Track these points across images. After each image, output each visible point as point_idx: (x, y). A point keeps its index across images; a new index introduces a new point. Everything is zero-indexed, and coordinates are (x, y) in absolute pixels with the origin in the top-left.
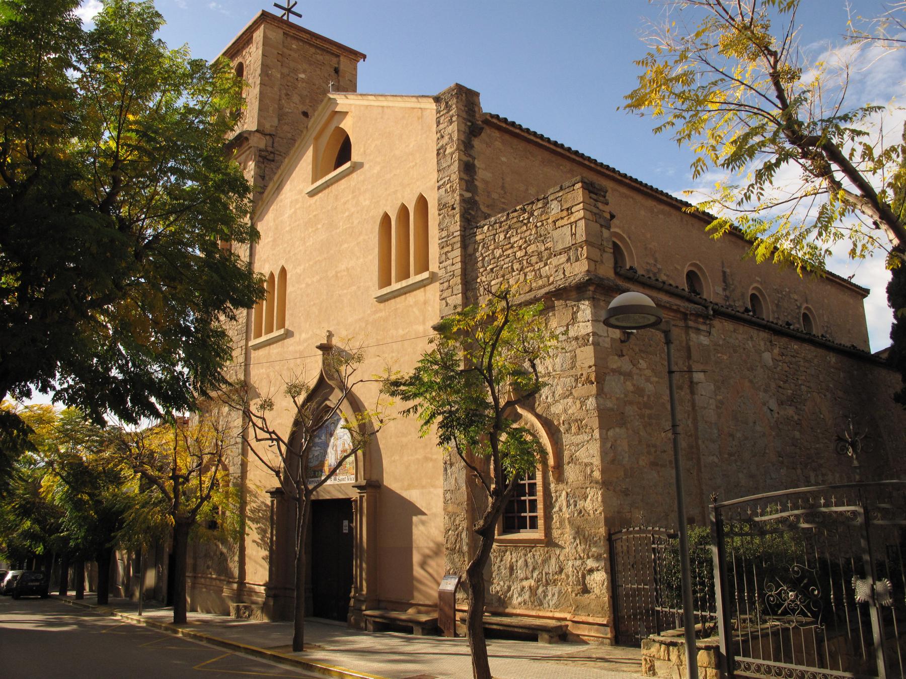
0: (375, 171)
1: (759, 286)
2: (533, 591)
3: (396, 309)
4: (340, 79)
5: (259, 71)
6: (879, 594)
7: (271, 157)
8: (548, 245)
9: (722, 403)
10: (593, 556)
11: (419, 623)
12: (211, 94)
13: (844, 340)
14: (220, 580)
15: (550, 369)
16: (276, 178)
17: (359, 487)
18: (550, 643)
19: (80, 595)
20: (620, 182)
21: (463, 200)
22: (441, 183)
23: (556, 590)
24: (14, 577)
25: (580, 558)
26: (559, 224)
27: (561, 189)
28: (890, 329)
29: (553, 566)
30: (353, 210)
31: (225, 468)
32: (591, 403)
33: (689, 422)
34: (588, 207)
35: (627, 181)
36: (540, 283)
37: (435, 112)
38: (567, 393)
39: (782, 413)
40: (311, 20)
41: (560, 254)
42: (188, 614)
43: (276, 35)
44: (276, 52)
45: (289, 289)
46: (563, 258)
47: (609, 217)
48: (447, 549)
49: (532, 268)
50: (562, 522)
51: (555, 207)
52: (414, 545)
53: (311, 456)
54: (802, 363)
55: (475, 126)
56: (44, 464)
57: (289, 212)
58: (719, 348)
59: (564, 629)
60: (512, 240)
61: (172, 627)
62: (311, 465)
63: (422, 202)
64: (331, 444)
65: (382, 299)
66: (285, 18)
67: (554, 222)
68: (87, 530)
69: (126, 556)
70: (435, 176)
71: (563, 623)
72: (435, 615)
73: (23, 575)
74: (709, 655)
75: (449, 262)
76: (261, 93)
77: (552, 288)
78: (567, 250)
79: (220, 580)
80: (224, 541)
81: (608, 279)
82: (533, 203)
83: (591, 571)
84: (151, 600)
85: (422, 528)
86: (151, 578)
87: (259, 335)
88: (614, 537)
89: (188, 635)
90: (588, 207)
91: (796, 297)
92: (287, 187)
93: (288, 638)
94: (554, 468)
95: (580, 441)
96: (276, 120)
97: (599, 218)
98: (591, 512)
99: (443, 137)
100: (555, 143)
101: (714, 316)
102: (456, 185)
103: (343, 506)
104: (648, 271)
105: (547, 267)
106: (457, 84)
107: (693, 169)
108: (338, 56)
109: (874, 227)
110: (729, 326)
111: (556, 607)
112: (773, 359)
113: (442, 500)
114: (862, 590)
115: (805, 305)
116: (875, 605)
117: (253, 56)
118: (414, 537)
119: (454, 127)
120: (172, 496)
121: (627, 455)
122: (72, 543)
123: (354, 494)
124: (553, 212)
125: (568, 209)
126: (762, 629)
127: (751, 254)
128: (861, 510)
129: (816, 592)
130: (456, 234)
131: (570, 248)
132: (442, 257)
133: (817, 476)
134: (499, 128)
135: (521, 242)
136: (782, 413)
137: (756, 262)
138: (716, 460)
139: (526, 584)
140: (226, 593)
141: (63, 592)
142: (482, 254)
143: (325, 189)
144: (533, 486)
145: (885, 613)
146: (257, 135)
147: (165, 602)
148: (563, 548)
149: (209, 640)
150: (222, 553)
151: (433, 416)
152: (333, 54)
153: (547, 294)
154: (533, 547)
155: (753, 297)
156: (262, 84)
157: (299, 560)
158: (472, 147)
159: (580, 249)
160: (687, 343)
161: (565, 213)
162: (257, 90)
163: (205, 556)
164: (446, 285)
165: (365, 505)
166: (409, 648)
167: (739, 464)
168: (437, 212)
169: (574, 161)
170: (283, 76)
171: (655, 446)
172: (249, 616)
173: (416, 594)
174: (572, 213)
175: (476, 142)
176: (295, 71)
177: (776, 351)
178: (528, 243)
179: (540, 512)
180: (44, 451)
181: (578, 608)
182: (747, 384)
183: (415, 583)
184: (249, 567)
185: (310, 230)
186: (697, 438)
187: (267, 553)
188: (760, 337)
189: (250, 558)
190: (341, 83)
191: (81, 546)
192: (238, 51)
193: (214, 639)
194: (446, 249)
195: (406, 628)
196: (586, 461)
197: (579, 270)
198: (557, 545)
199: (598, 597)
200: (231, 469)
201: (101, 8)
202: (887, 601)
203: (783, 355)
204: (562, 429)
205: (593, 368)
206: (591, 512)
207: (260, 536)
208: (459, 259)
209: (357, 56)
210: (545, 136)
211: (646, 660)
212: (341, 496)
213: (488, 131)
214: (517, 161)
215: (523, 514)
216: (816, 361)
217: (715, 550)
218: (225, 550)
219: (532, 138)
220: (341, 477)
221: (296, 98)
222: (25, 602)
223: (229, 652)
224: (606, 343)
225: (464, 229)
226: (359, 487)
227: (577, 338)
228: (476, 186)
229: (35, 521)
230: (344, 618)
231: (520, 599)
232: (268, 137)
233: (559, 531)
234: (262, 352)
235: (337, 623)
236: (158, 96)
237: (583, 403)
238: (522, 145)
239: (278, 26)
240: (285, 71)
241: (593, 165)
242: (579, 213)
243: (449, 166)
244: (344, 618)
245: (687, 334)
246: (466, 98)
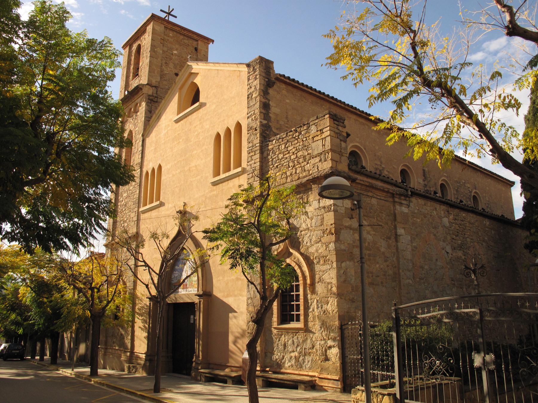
0: (213, 108)
1: (446, 179)
2: (297, 359)
3: (222, 190)
4: (198, 54)
5: (149, 49)
6: (488, 363)
7: (155, 100)
8: (310, 152)
9: (416, 248)
10: (331, 338)
11: (230, 377)
12: (100, 59)
13: (498, 213)
14: (120, 350)
15: (309, 225)
16: (157, 112)
17: (198, 295)
18: (305, 390)
19: (42, 359)
20: (360, 116)
21: (262, 125)
22: (249, 115)
23: (310, 358)
24: (5, 347)
25: (324, 339)
26: (315, 139)
27: (317, 118)
28: (522, 205)
29: (308, 344)
30: (200, 131)
31: (124, 283)
32: (332, 246)
33: (394, 259)
34: (332, 129)
35: (364, 115)
36: (304, 174)
37: (247, 73)
38: (318, 240)
39: (454, 254)
40: (182, 20)
41: (316, 157)
42: (99, 370)
43: (160, 28)
44: (160, 38)
45: (163, 178)
46: (317, 159)
47: (345, 135)
48: (248, 333)
49: (300, 165)
50: (314, 318)
51: (313, 129)
52: (230, 331)
53: (173, 277)
54: (468, 225)
55: (270, 79)
56: (20, 280)
57: (164, 132)
58: (415, 215)
59: (314, 382)
60: (289, 149)
61: (88, 377)
62: (173, 282)
63: (239, 126)
64: (184, 270)
65: (215, 184)
66: (167, 18)
67: (313, 138)
68: (45, 320)
69: (69, 335)
70: (246, 110)
71: (314, 379)
72: (240, 373)
73: (9, 346)
74: (390, 398)
75: (253, 162)
76: (150, 61)
77: (311, 177)
79: (120, 350)
80: (123, 327)
81: (344, 172)
82: (301, 127)
83: (330, 347)
84: (82, 361)
85: (234, 320)
86: (82, 349)
87: (145, 205)
88: (344, 327)
89: (96, 382)
90: (332, 129)
91: (469, 186)
92: (163, 117)
93: (151, 385)
94: (310, 285)
95: (325, 269)
96: (159, 78)
97: (340, 136)
98: (331, 312)
99: (251, 87)
100: (320, 92)
101: (411, 195)
102: (258, 116)
103: (190, 307)
104: (376, 169)
105: (308, 165)
106: (260, 57)
107: (368, 101)
109: (480, 137)
110: (421, 201)
111: (310, 369)
112: (449, 222)
113: (246, 304)
114: (478, 360)
115: (474, 191)
116: (485, 369)
117: (146, 40)
118: (230, 326)
119: (257, 82)
120: (90, 299)
121: (354, 278)
122: (36, 328)
123: (196, 300)
124: (312, 132)
125: (321, 130)
126: (426, 384)
127: (410, 155)
128: (478, 311)
129: (452, 361)
130: (257, 145)
131: (321, 153)
132: (249, 160)
135: (294, 150)
136: (454, 254)
137: (414, 159)
138: (411, 282)
139: (293, 354)
140: (123, 358)
141: (33, 357)
142: (272, 157)
143: (184, 118)
144: (298, 296)
145: (490, 373)
146: (148, 86)
148: (314, 333)
149: (108, 386)
150: (122, 334)
151: (227, 251)
152: (194, 39)
153: (307, 180)
154: (297, 333)
155: (442, 186)
157: (158, 338)
158: (268, 93)
159: (327, 154)
160: (394, 212)
161: (319, 133)
162: (148, 60)
163: (112, 336)
164: (251, 175)
165: (202, 306)
166: (222, 392)
167: (426, 284)
168: (247, 132)
169: (331, 102)
171: (372, 273)
172: (135, 372)
173: (230, 360)
174: (323, 133)
175: (271, 91)
176: (171, 49)
177: (451, 217)
178: (298, 150)
179: (302, 312)
180: (20, 272)
181: (322, 370)
182: (432, 236)
183: (230, 353)
184: (137, 343)
185: (176, 143)
186: (399, 269)
187: (147, 334)
188: (441, 209)
189: (137, 337)
190: (199, 57)
191: (42, 329)
192: (138, 37)
193: (111, 384)
194: (251, 154)
195: (223, 380)
196: (328, 281)
198: (311, 332)
199: (333, 363)
200: (128, 284)
201: (33, 8)
202: (492, 367)
203: (455, 219)
204: (315, 261)
205: (334, 225)
206: (331, 312)
207: (143, 324)
208: (258, 160)
209: (208, 41)
210: (313, 88)
211: (354, 401)
212: (189, 301)
213: (278, 84)
214: (296, 102)
215: (292, 313)
216: (476, 224)
217: (394, 334)
218: (123, 333)
219: (305, 88)
220: (190, 289)
221: (171, 65)
222: (10, 362)
223: (117, 392)
224: (342, 210)
225: (261, 142)
226: (198, 295)
227: (324, 207)
228: (270, 117)
229: (18, 314)
230: (189, 374)
231: (289, 364)
232: (154, 88)
233: (313, 323)
234: (146, 215)
235: (186, 377)
236: (68, 60)
237: (327, 246)
238: (299, 93)
239: (163, 25)
240: (165, 49)
241: (343, 105)
242: (327, 132)
243: (254, 105)
244: (189, 374)
245: (394, 206)
246: (265, 65)
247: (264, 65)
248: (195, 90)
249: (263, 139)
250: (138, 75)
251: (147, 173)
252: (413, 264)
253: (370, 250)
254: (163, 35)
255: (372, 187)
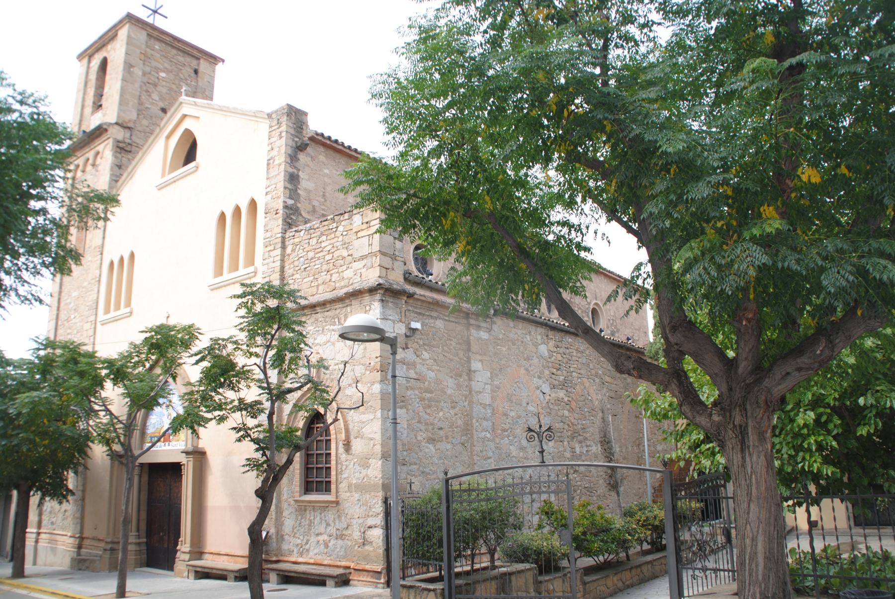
4: (199, 79)
7: (128, 148)
9: (499, 388)
21: (286, 207)
26: (360, 234)
33: (466, 404)
36: (342, 284)
39: (553, 395)
43: (142, 36)
44: (138, 51)
46: (360, 264)
60: (323, 245)
63: (253, 204)
65: (214, 288)
70: (264, 183)
75: (271, 260)
78: (363, 258)
81: (398, 284)
99: (272, 149)
101: (494, 315)
108: (198, 59)
115: (595, 301)
117: (117, 53)
119: (283, 141)
121: (406, 432)
123: (182, 459)
133: (582, 447)
134: (324, 145)
136: (553, 395)
146: (116, 127)
147: (9, 558)
152: (193, 56)
156: (124, 80)
170: (144, 74)
171: (432, 424)
177: (552, 343)
182: (523, 371)
186: (472, 418)
190: (200, 84)
196: (371, 436)
197: (372, 277)
203: (557, 347)
209: (214, 60)
221: (155, 96)
232: (126, 130)
240: (148, 69)
246: (296, 117)
247: (293, 118)
248: (191, 141)
249: (287, 227)
250: (101, 106)
251: (112, 263)
252: (493, 410)
253: (431, 392)
254: (144, 47)
255: (436, 303)
